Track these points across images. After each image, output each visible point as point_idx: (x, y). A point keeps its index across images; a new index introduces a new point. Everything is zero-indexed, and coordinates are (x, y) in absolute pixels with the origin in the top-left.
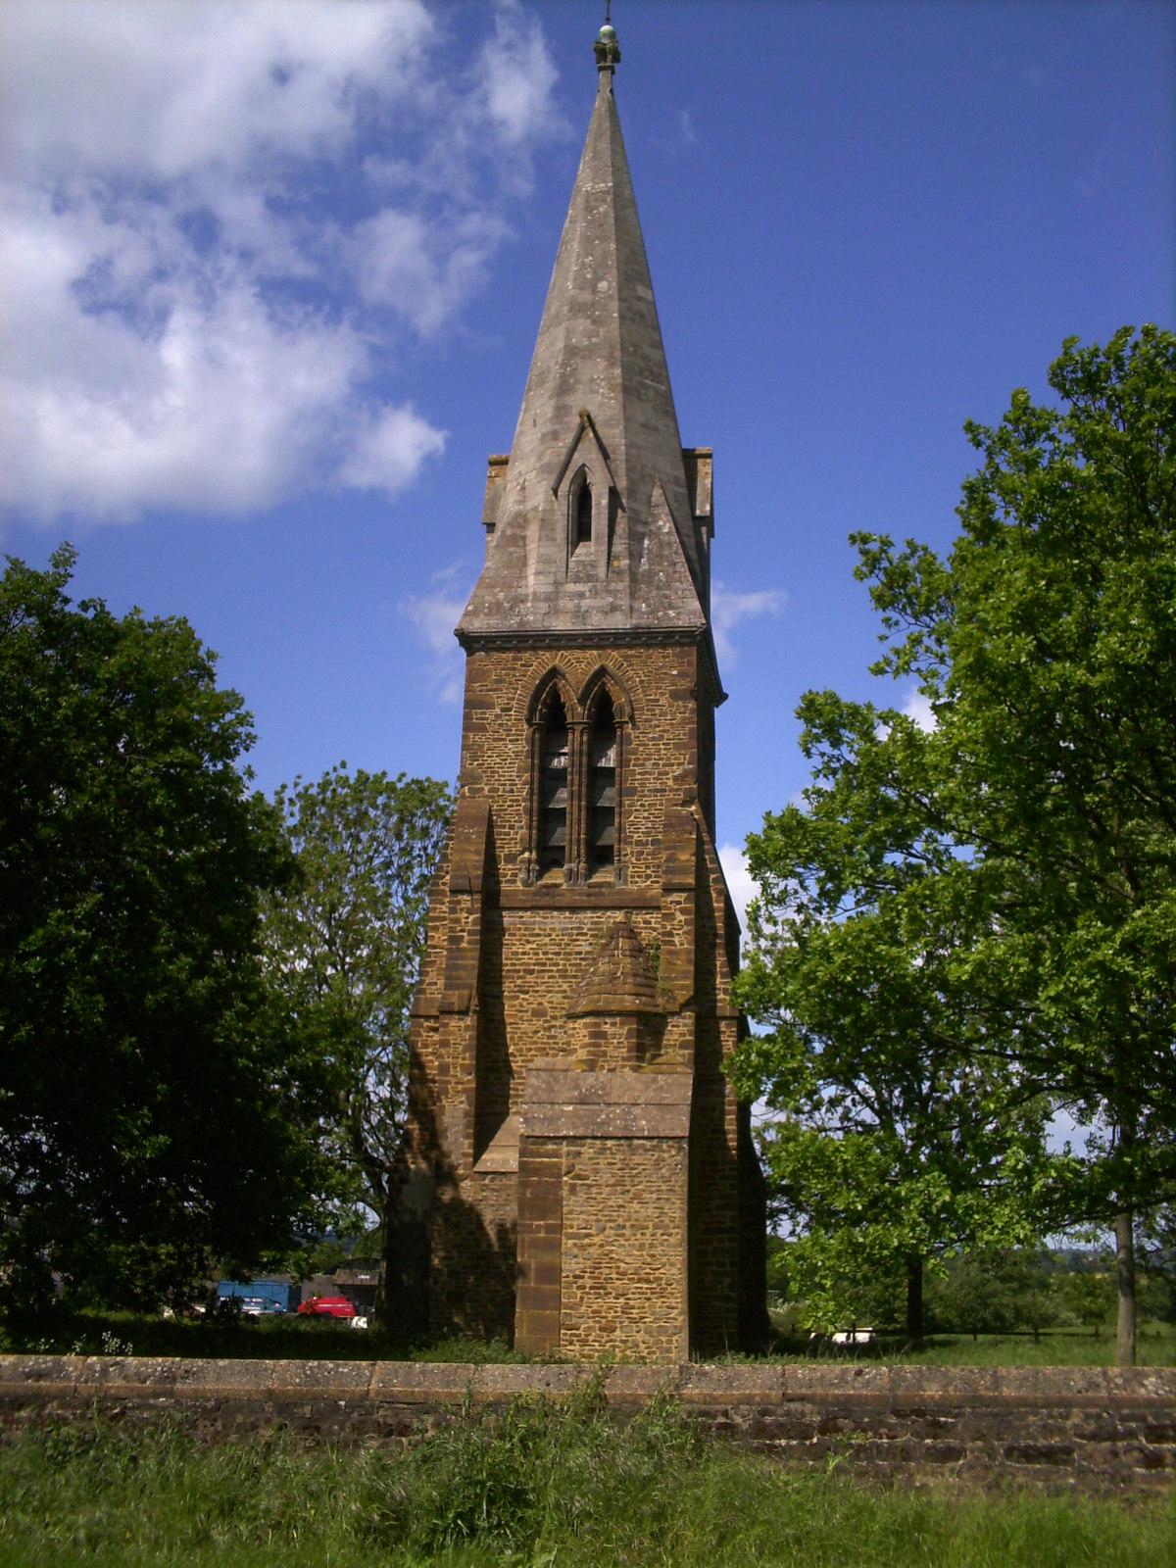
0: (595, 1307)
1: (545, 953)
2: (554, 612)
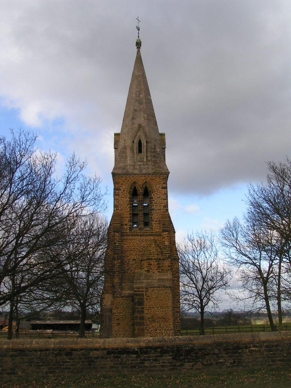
0: (153, 325)
1: (135, 246)
2: (135, 169)
